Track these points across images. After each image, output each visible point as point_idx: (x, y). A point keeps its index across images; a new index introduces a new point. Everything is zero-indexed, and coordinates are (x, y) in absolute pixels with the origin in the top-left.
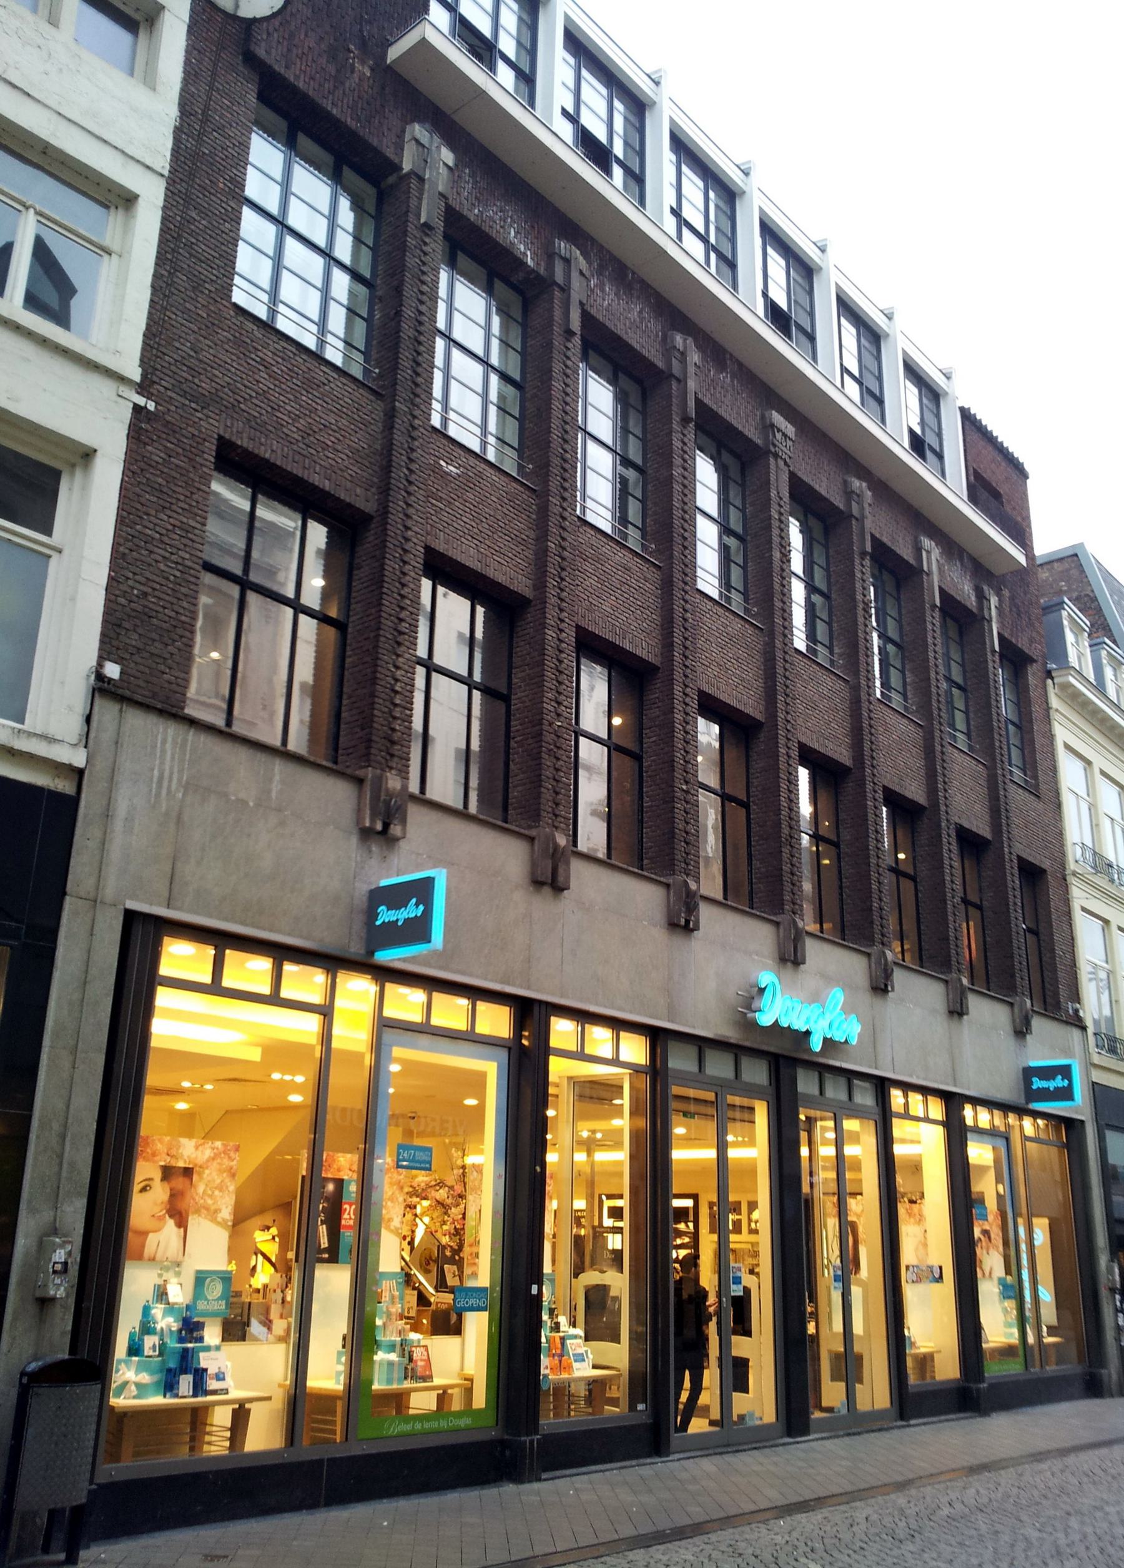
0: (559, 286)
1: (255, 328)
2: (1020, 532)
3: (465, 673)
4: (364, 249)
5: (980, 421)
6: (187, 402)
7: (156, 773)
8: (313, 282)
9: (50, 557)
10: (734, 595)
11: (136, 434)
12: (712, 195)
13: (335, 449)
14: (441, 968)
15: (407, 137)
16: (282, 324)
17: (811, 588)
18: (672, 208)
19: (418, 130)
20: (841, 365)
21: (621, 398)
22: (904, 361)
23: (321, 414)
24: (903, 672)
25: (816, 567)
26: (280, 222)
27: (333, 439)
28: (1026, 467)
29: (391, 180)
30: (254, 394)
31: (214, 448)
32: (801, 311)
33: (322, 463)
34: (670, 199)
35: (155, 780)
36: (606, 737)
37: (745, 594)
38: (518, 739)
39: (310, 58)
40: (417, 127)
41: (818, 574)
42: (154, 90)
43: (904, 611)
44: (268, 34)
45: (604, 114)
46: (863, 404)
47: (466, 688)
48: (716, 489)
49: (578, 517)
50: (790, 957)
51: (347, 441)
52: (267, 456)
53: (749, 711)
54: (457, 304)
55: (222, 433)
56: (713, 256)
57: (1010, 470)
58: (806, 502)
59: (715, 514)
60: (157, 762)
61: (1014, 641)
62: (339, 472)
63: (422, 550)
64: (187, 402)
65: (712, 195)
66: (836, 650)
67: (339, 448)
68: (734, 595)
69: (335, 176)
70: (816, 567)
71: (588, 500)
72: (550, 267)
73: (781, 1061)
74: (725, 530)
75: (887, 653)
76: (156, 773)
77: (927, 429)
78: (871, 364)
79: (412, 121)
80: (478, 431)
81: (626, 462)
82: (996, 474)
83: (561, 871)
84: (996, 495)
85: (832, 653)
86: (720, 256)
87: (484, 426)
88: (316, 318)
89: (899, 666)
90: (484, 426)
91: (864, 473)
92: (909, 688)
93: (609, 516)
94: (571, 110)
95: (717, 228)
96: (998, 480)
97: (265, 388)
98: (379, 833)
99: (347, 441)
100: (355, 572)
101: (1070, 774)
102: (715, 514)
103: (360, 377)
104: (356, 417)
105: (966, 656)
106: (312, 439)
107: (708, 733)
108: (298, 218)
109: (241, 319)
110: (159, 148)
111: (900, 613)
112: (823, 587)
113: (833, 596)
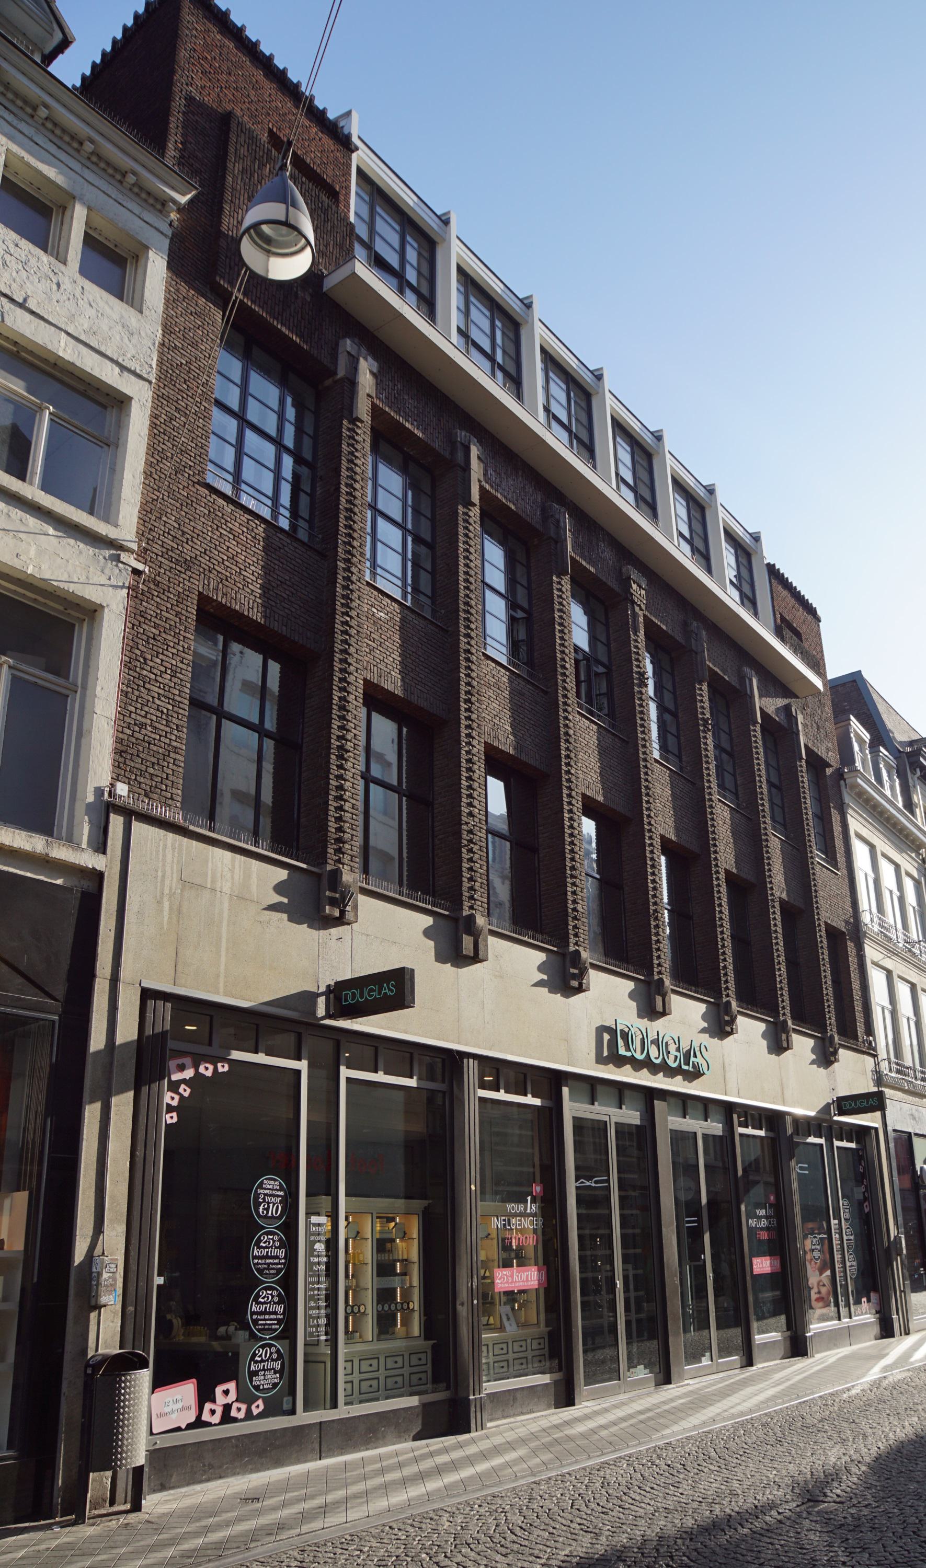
0: (461, 467)
1: (225, 504)
2: (817, 665)
3: (255, 719)
4: (423, 519)
5: (783, 574)
6: (174, 566)
7: (160, 874)
8: (266, 464)
9: (68, 696)
10: (301, 523)
11: (135, 593)
12: (498, 323)
13: (289, 601)
14: (389, 1029)
15: (340, 349)
16: (244, 500)
17: (661, 708)
18: (458, 328)
19: (348, 344)
20: (617, 474)
21: (412, 483)
22: (672, 476)
23: (277, 572)
24: (734, 775)
25: (665, 691)
26: (240, 417)
27: (287, 592)
28: (819, 612)
29: (328, 382)
30: (225, 558)
31: (195, 602)
32: (580, 427)
33: (281, 613)
34: (541, 400)
35: (159, 879)
36: (257, 722)
37: (310, 522)
38: (441, 837)
39: (263, 287)
40: (348, 342)
41: (668, 696)
42: (141, 312)
43: (733, 727)
44: (230, 268)
45: (487, 329)
46: (637, 506)
47: (396, 795)
48: (503, 569)
49: (368, 584)
50: (457, 944)
51: (299, 594)
52: (237, 608)
53: (533, 762)
54: (381, 481)
55: (201, 590)
56: (575, 442)
57: (810, 617)
58: (498, 521)
59: (502, 590)
60: (160, 865)
61: (816, 750)
62: (293, 619)
63: (362, 682)
64: (174, 566)
65: (498, 323)
66: (684, 758)
67: (293, 600)
68: (301, 523)
69: (283, 382)
70: (665, 691)
71: (488, 638)
72: (453, 452)
73: (689, 1103)
74: (512, 605)
75: (721, 760)
76: (160, 874)
77: (694, 535)
78: (644, 476)
79: (344, 337)
80: (399, 583)
81: (417, 540)
82: (798, 617)
83: (481, 946)
84: (798, 634)
85: (681, 761)
86: (580, 441)
87: (275, 498)
88: (270, 494)
89: (731, 771)
90: (275, 498)
91: (560, 497)
92: (739, 788)
93: (504, 650)
94: (463, 328)
95: (577, 419)
96: (798, 619)
97: (235, 553)
98: (337, 918)
99: (299, 594)
100: (307, 702)
101: (861, 853)
102: (502, 590)
103: (306, 540)
104: (305, 574)
105: (781, 763)
106: (271, 593)
107: (588, 827)
108: (254, 413)
109: (214, 496)
110: (146, 356)
111: (730, 727)
112: (671, 706)
113: (680, 715)
